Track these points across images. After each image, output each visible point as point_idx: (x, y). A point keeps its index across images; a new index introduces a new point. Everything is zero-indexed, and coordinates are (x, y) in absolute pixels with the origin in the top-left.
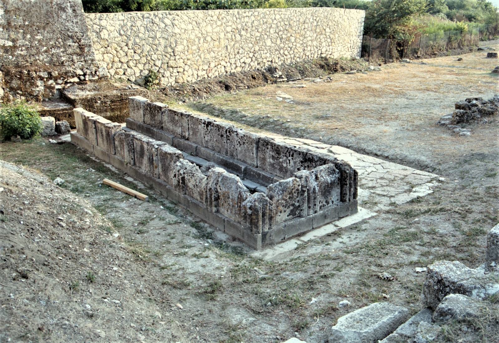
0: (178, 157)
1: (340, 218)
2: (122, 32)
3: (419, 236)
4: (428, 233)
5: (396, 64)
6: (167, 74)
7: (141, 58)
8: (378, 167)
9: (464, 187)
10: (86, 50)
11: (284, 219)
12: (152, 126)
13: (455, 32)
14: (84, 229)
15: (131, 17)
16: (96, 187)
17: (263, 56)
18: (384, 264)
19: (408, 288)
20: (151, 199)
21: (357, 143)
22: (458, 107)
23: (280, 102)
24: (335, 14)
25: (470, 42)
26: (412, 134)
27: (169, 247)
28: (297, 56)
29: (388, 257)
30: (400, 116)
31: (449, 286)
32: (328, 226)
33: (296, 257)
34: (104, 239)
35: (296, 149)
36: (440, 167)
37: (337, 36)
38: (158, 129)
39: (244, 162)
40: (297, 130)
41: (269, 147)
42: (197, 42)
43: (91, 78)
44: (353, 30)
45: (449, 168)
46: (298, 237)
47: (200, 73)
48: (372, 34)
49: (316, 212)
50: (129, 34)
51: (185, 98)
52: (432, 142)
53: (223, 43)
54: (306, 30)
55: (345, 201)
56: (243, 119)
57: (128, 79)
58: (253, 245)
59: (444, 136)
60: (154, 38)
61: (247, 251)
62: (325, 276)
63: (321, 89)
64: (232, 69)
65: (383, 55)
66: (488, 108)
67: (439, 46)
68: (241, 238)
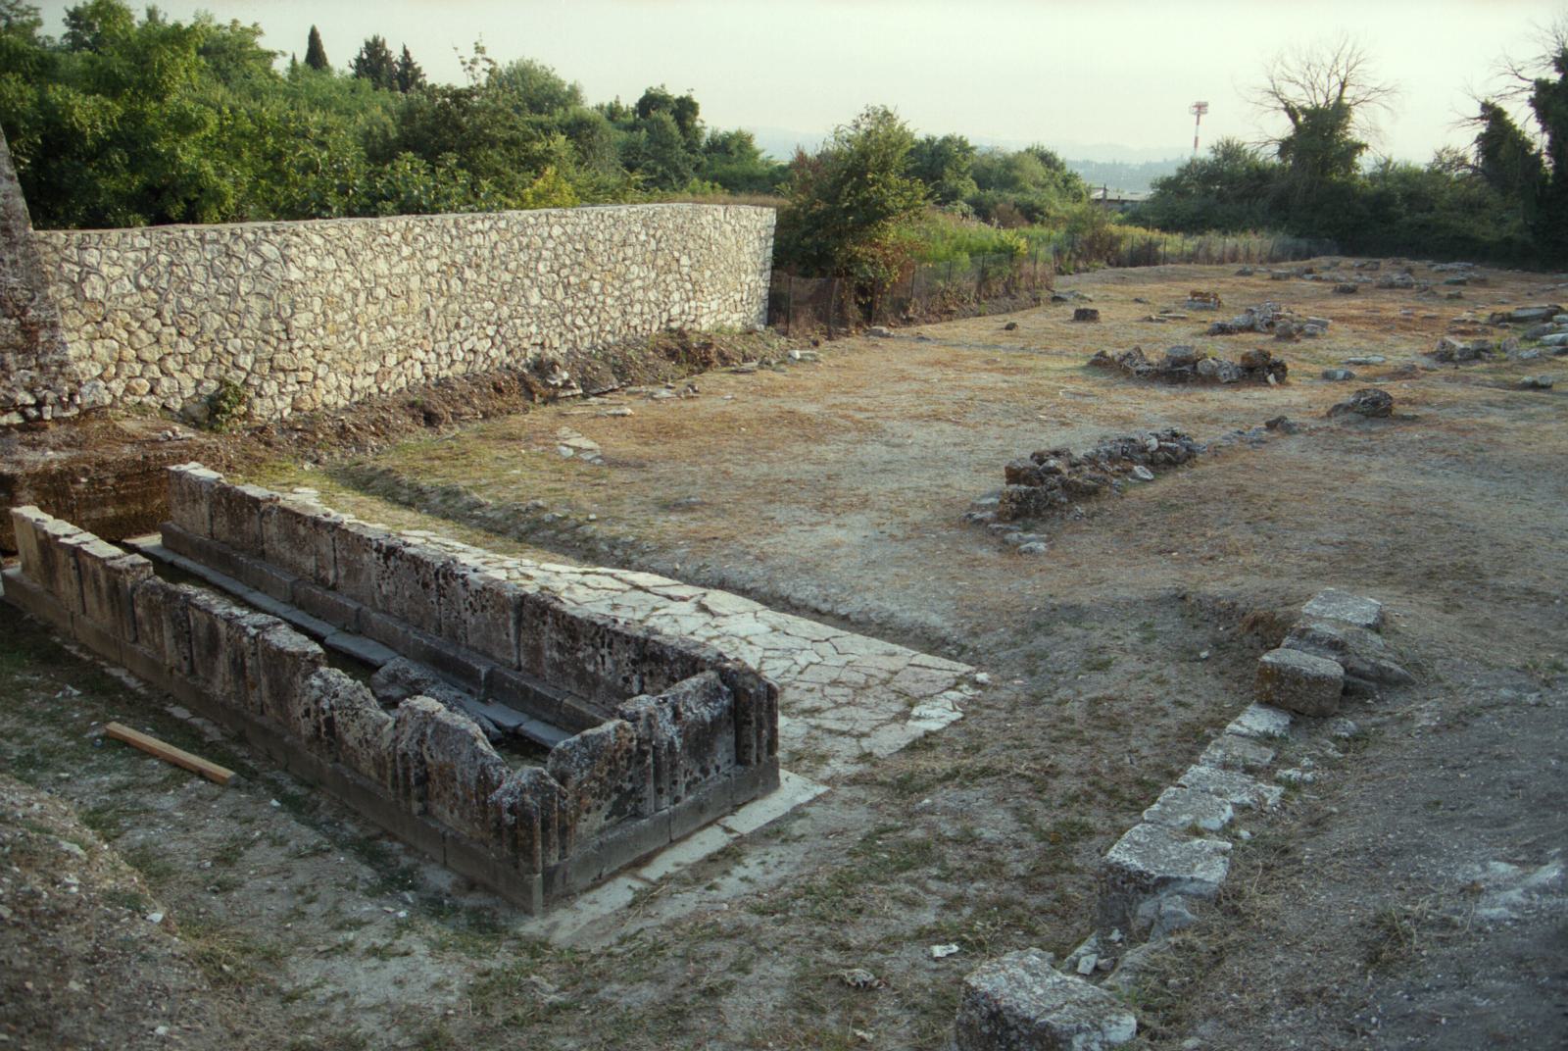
0: (314, 663)
2: (144, 282)
3: (935, 852)
4: (957, 842)
5: (856, 341)
6: (271, 388)
7: (197, 347)
9: (1036, 700)
10: (43, 336)
11: (596, 827)
14: (63, 913)
15: (169, 241)
16: (88, 748)
17: (521, 332)
18: (854, 943)
19: (915, 1006)
20: (248, 777)
21: (769, 580)
22: (1014, 475)
23: (567, 460)
25: (1033, 279)
26: (905, 549)
27: (303, 927)
28: (608, 328)
29: (862, 919)
30: (872, 496)
31: (1016, 1027)
32: (709, 830)
35: (617, 627)
36: (977, 643)
37: (708, 273)
39: (488, 655)
40: (614, 542)
41: (549, 620)
42: (349, 303)
43: (58, 413)
44: (747, 258)
45: (998, 645)
47: (358, 383)
49: (677, 800)
50: (165, 286)
51: (320, 452)
52: (955, 571)
54: (627, 263)
64: (441, 369)
65: (823, 317)
66: (1085, 477)
67: (958, 292)
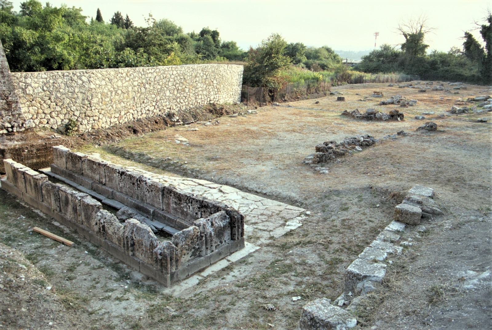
1: (231, 253)
2: (45, 88)
3: (294, 268)
4: (300, 264)
5: (269, 107)
6: (85, 122)
7: (62, 109)
8: (259, 204)
10: (14, 105)
11: (187, 260)
12: (73, 172)
13: (312, 80)
14: (20, 287)
15: (53, 76)
17: (164, 104)
18: (268, 296)
19: (287, 316)
20: (78, 244)
21: (241, 182)
22: (318, 149)
24: (221, 69)
25: (324, 88)
26: (284, 173)
27: (95, 291)
29: (271, 288)
30: (273, 156)
31: (319, 323)
32: (222, 261)
33: (198, 292)
34: (38, 294)
35: (194, 197)
36: (306, 202)
37: (222, 86)
38: (79, 174)
40: (193, 170)
41: (172, 195)
43: (18, 129)
45: (313, 202)
46: (199, 273)
47: (112, 120)
48: (249, 83)
49: (212, 251)
50: (52, 90)
51: (100, 142)
52: (300, 179)
53: (131, 95)
54: (197, 82)
55: (234, 240)
56: (149, 161)
57: (51, 128)
58: (164, 283)
59: (308, 174)
60: (73, 93)
61: (159, 289)
62: (223, 311)
63: (211, 132)
65: (258, 100)
66: (340, 150)
67: (301, 92)
68: (153, 277)
